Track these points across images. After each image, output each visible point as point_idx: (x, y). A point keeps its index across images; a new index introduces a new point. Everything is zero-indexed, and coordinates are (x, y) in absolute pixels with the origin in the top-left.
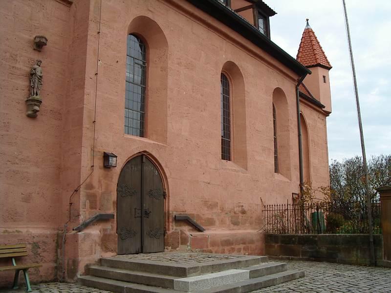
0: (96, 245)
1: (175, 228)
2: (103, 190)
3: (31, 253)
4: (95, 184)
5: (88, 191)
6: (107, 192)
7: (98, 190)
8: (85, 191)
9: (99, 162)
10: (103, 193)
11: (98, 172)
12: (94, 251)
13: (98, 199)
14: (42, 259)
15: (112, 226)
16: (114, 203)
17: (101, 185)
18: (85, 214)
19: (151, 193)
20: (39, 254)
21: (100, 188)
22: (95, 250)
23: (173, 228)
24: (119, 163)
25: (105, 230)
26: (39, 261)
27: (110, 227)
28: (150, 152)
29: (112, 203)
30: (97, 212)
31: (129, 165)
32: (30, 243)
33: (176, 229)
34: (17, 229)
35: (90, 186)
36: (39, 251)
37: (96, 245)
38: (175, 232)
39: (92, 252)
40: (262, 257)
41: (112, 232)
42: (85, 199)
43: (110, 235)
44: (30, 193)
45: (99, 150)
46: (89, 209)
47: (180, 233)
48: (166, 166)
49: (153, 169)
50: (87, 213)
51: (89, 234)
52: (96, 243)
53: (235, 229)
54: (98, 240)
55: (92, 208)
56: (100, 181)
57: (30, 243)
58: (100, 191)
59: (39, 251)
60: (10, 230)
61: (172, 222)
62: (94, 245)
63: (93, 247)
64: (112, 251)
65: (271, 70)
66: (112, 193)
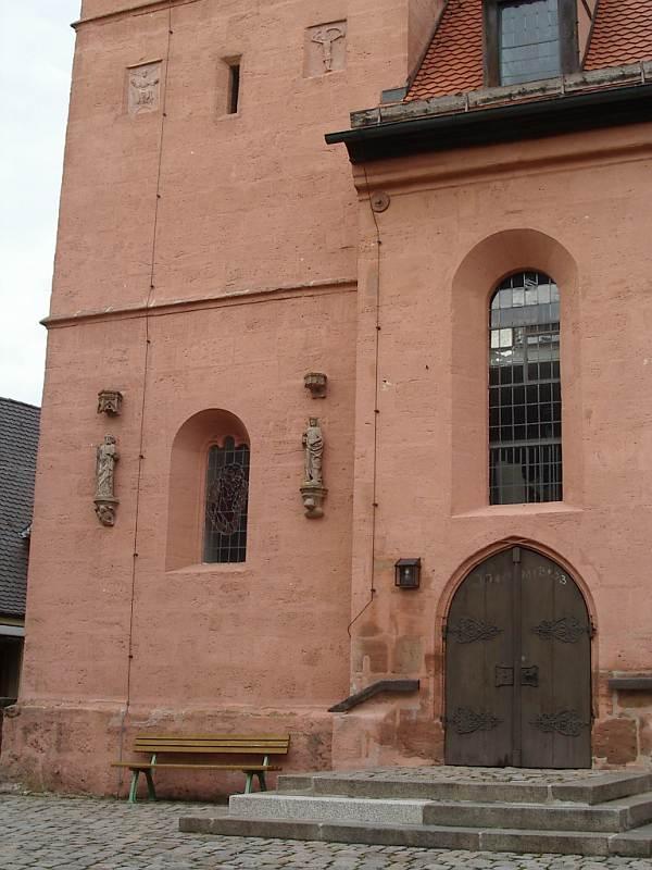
0: (368, 741)
1: (617, 709)
2: (400, 635)
3: (305, 751)
4: (383, 622)
5: (366, 638)
6: (412, 637)
7: (389, 635)
8: (361, 638)
9: (387, 581)
10: (399, 641)
11: (389, 598)
12: (364, 751)
13: (389, 652)
14: (326, 763)
15: (422, 705)
16: (428, 657)
17: (396, 626)
18: (361, 681)
19: (545, 632)
20: (321, 755)
21: (394, 631)
22: (367, 749)
23: (609, 711)
24: (440, 575)
25: (405, 713)
26: (319, 766)
27: (418, 707)
28: (528, 537)
29: (423, 657)
30: (381, 677)
31: (478, 574)
32: (305, 735)
33: (621, 715)
34: (293, 711)
35: (371, 629)
36: (321, 748)
37: (368, 741)
38: (620, 722)
39: (360, 753)
40: (429, 802)
41: (421, 717)
42: (360, 654)
43: (418, 723)
44: (316, 650)
45: (391, 557)
46: (369, 670)
47: (638, 723)
48: (584, 562)
49: (553, 573)
50: (365, 678)
51: (356, 718)
52: (368, 735)
53: (189, 718)
54: (373, 730)
55: (375, 669)
56: (392, 617)
57: (305, 735)
58: (394, 637)
59: (321, 748)
60: (281, 712)
61: (609, 696)
62: (364, 740)
63: (364, 746)
64: (422, 756)
65: (497, 182)
66: (422, 639)
